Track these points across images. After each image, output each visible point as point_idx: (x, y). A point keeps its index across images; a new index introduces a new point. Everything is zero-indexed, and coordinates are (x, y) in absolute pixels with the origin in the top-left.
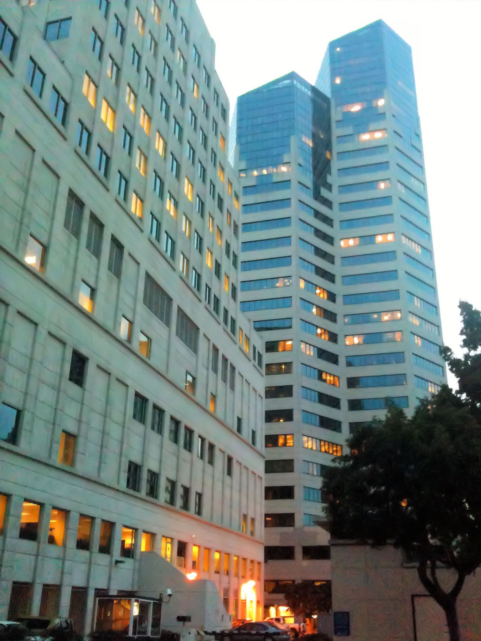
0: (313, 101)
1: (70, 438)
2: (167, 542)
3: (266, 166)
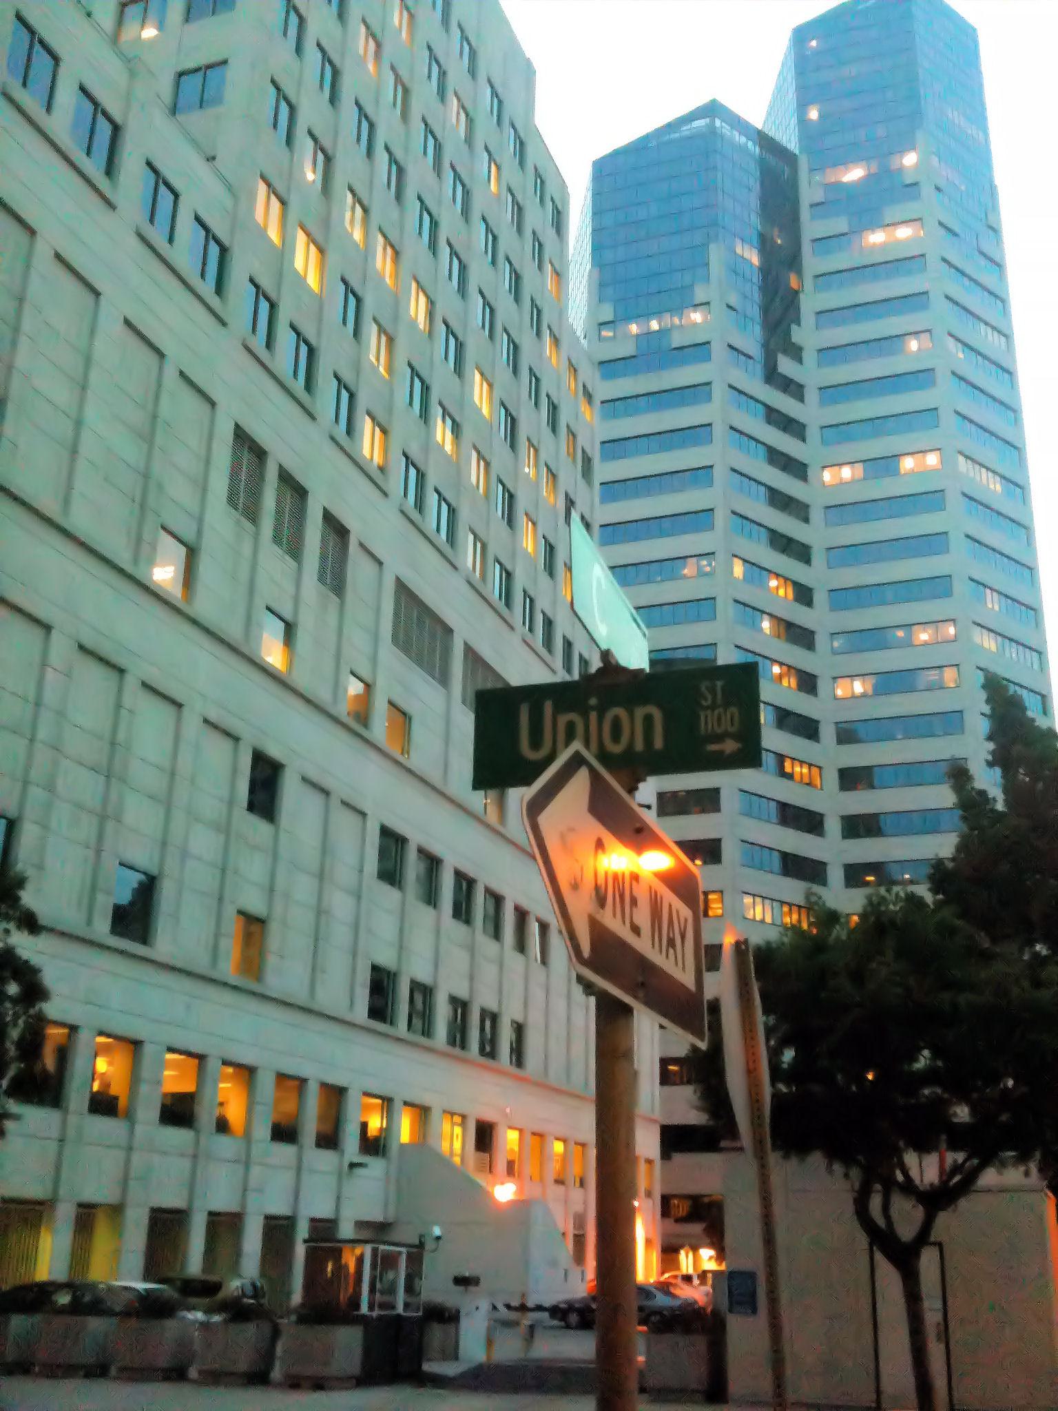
0: (762, 163)
1: (254, 925)
2: (453, 1124)
3: (658, 314)
